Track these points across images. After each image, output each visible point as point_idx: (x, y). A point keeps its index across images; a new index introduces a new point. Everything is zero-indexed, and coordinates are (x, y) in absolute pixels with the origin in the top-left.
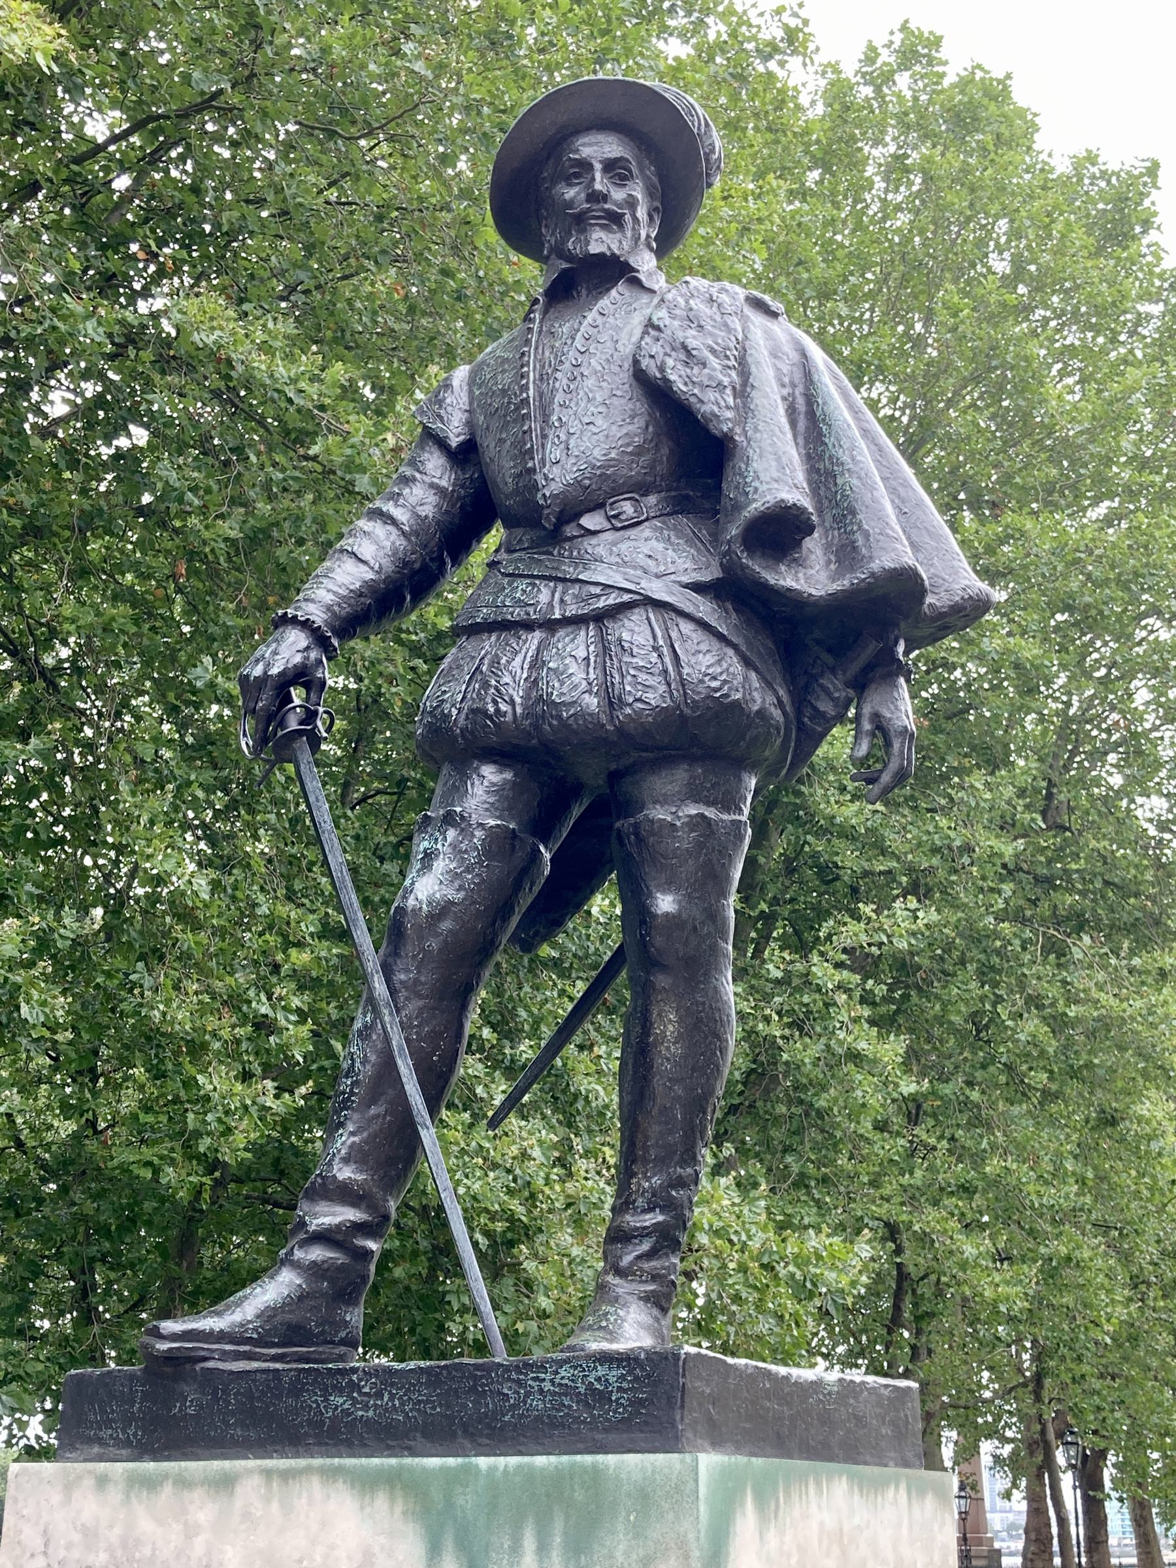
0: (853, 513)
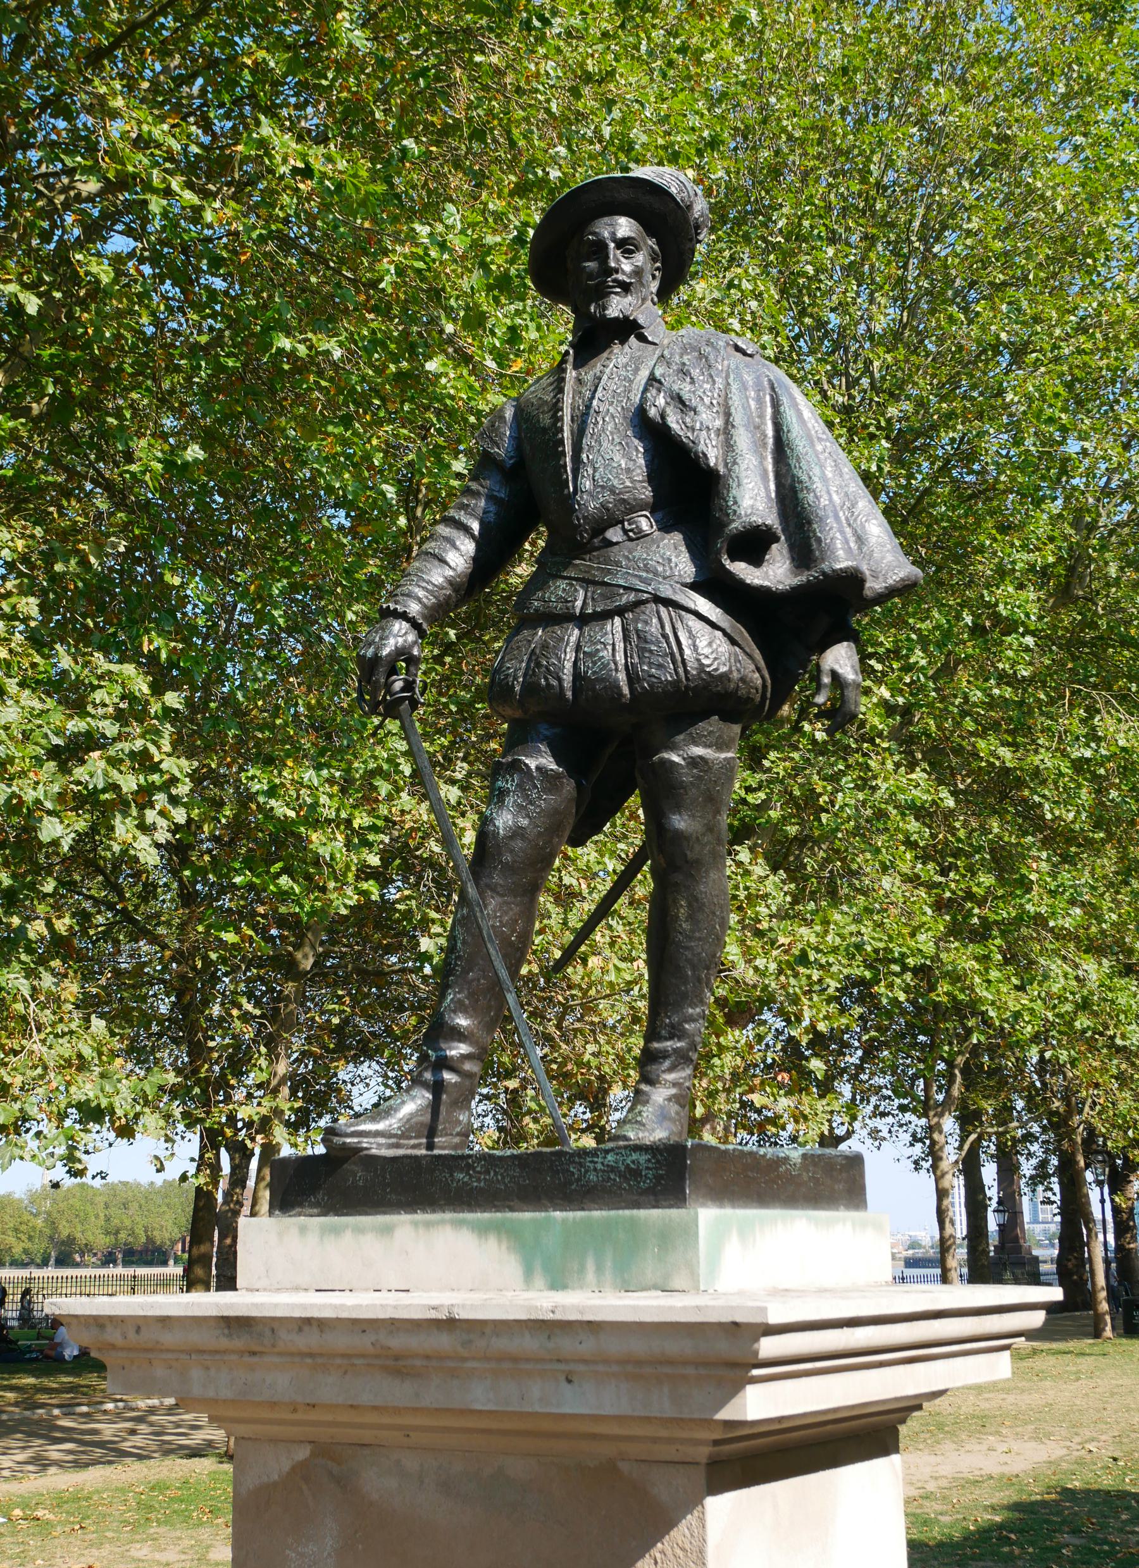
0: (810, 523)
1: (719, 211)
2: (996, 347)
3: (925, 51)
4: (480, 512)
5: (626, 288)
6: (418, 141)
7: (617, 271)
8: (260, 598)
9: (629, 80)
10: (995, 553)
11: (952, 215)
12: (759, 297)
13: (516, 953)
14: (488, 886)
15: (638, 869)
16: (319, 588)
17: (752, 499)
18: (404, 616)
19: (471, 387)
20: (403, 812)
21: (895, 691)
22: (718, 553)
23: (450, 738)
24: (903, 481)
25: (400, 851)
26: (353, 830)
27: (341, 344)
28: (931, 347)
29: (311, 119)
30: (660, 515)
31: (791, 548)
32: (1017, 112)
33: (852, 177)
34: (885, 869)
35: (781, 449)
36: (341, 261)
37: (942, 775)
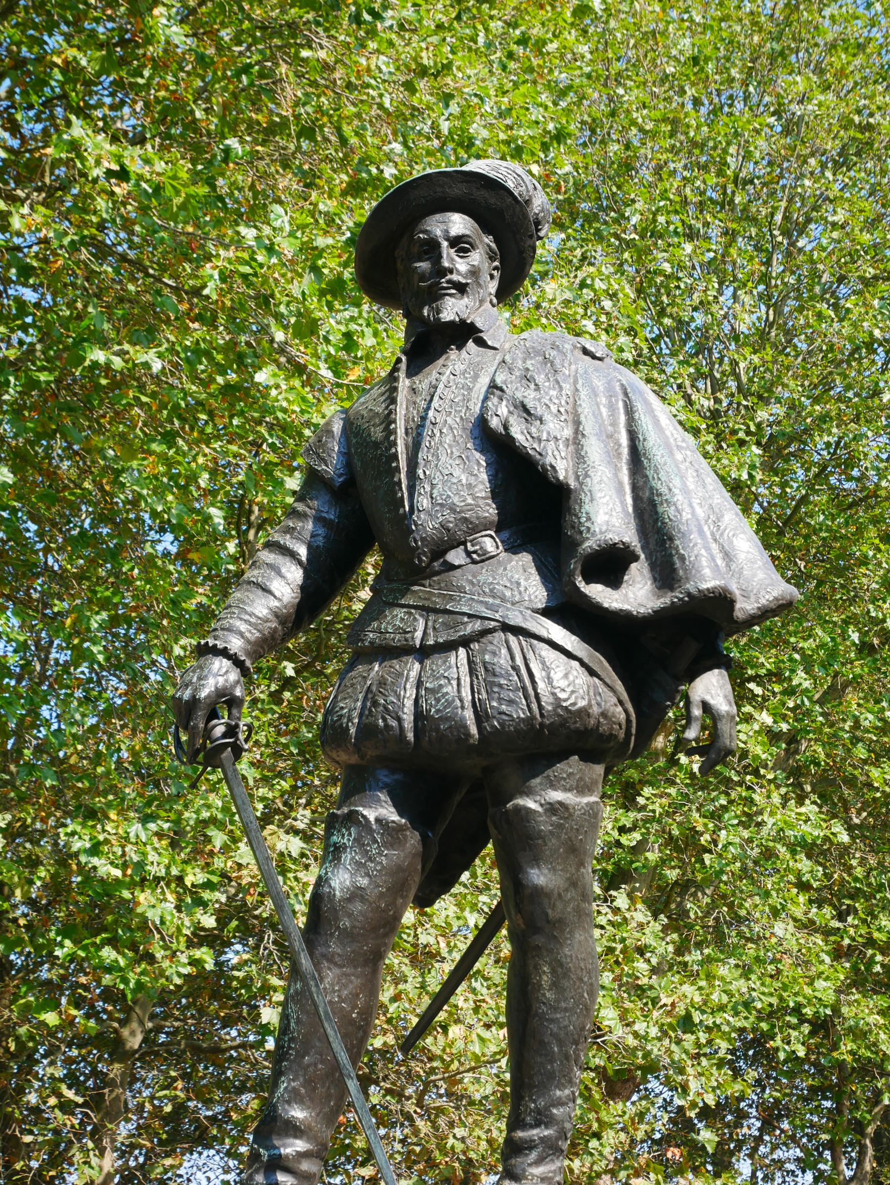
0: (671, 539)
1: (569, 207)
2: (870, 345)
3: (778, 39)
4: (307, 536)
5: (461, 289)
6: (242, 142)
7: (451, 272)
8: (78, 633)
9: (468, 74)
10: (879, 564)
11: (816, 208)
12: (613, 296)
13: (357, 1032)
14: (324, 956)
15: (497, 929)
16: (143, 620)
17: (607, 516)
18: (224, 653)
19: (304, 399)
20: (240, 866)
21: (779, 717)
22: (572, 574)
23: (291, 782)
24: (778, 491)
25: (238, 909)
26: (185, 887)
27: (160, 356)
28: (803, 346)
29: (127, 121)
30: (506, 534)
31: (653, 567)
32: (879, 100)
33: (708, 172)
34: (775, 913)
35: (637, 458)
36: (163, 269)
37: (835, 809)
